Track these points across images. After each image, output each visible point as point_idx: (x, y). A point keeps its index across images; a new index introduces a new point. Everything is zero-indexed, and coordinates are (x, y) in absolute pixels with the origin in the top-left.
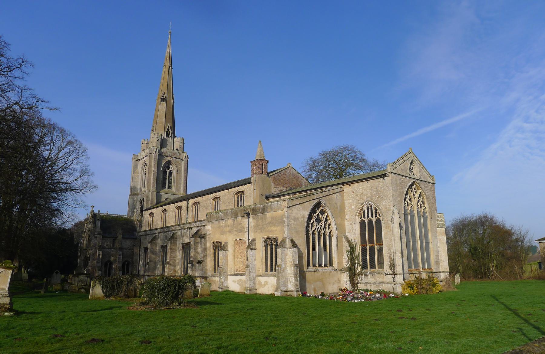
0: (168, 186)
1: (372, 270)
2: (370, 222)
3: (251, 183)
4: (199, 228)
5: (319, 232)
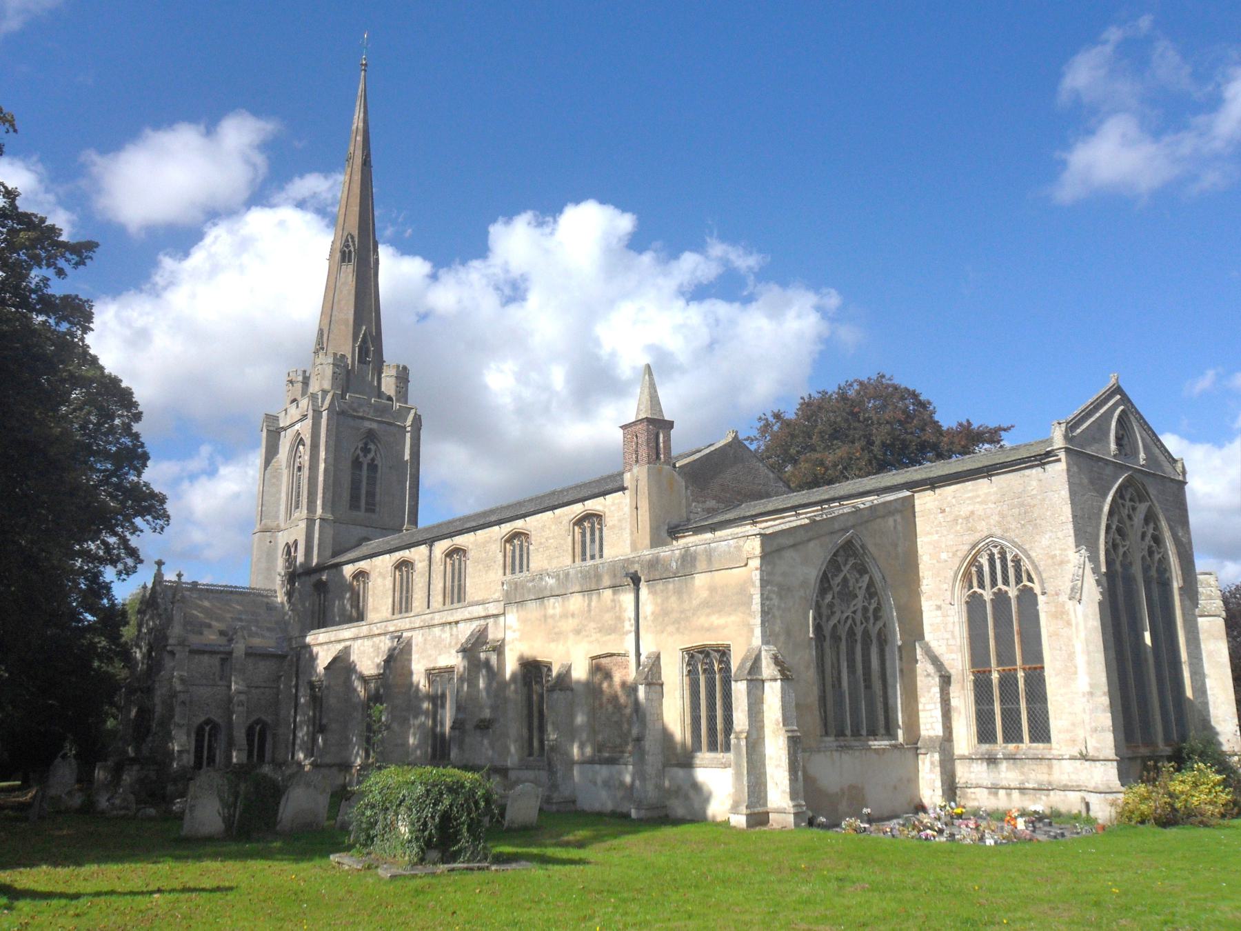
0: (367, 503)
1: (1011, 747)
2: (1001, 600)
3: (623, 489)
4: (348, 643)
5: (851, 633)
